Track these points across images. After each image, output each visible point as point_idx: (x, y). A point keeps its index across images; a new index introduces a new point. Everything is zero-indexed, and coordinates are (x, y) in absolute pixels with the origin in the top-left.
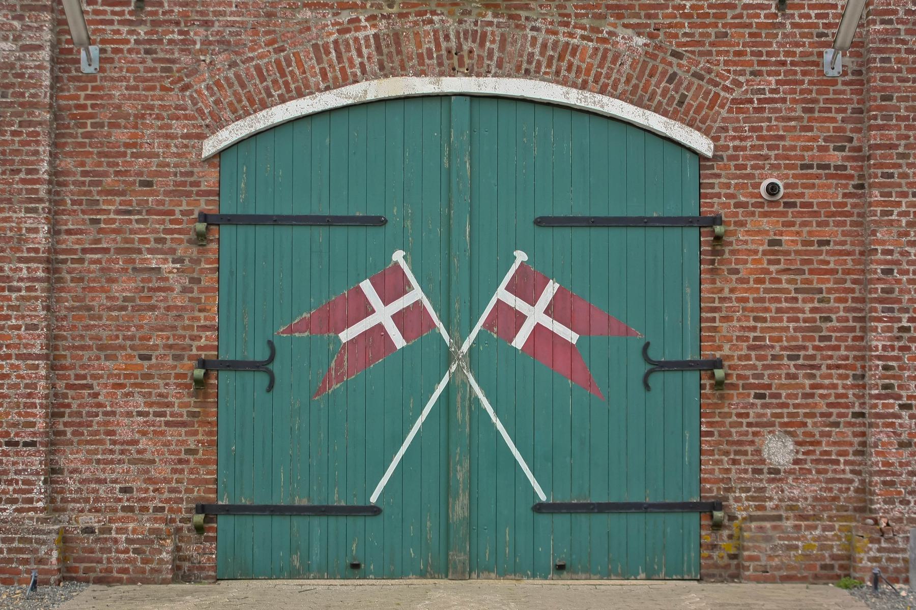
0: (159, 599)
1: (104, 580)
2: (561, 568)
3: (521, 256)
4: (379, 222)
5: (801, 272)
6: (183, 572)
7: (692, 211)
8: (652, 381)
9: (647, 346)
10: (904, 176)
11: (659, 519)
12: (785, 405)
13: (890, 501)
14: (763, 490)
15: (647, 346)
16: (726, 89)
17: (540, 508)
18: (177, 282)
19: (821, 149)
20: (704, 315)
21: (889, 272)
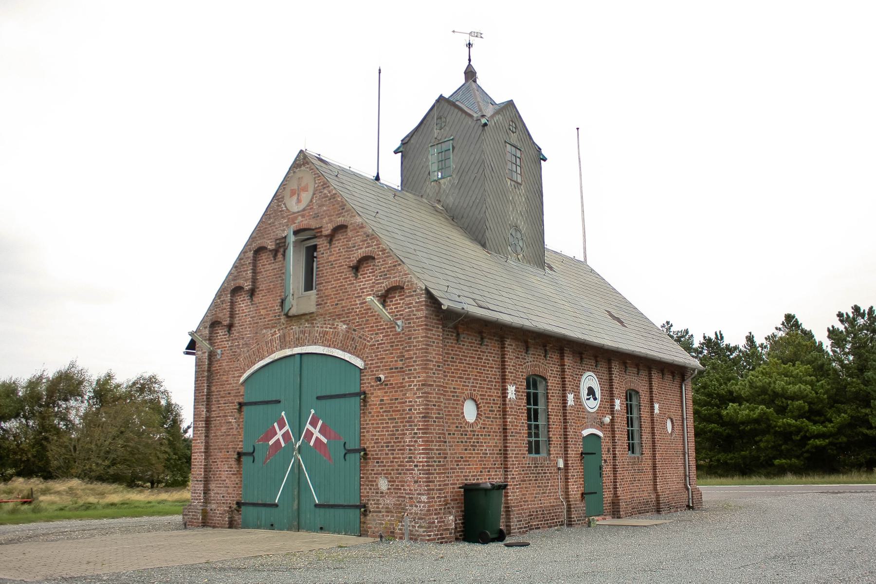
0: (106, 531)
1: (214, 527)
3: (313, 411)
5: (389, 411)
6: (232, 525)
7: (358, 390)
10: (415, 370)
11: (348, 511)
12: (385, 466)
13: (411, 506)
17: (316, 506)
18: (235, 425)
19: (396, 361)
21: (410, 410)
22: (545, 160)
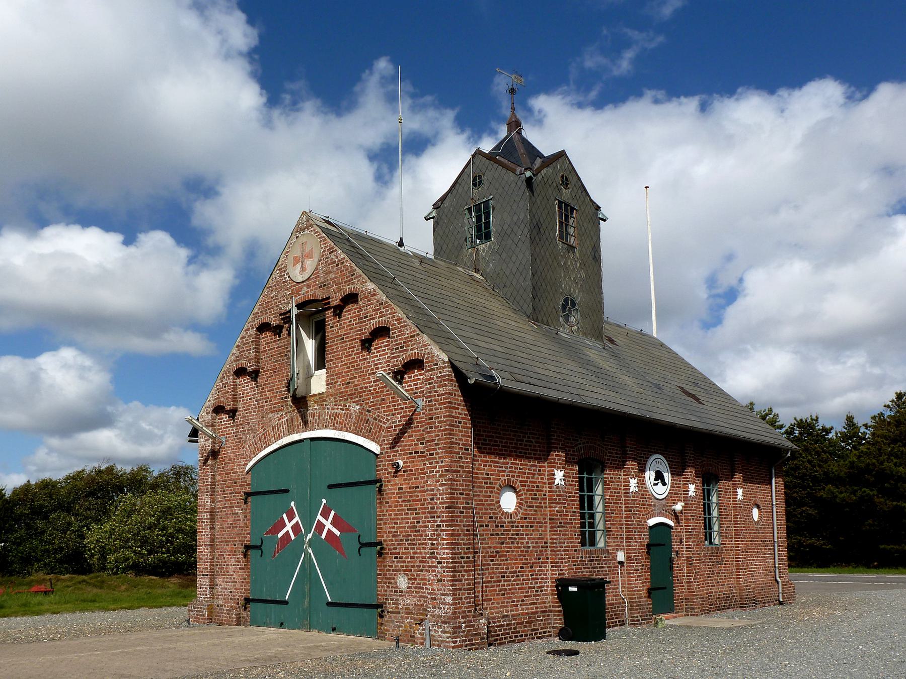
2: (334, 629)
3: (324, 501)
4: (286, 491)
12: (404, 562)
13: (434, 607)
14: (397, 600)
16: (384, 423)
17: (329, 604)
18: (242, 517)
21: (432, 499)
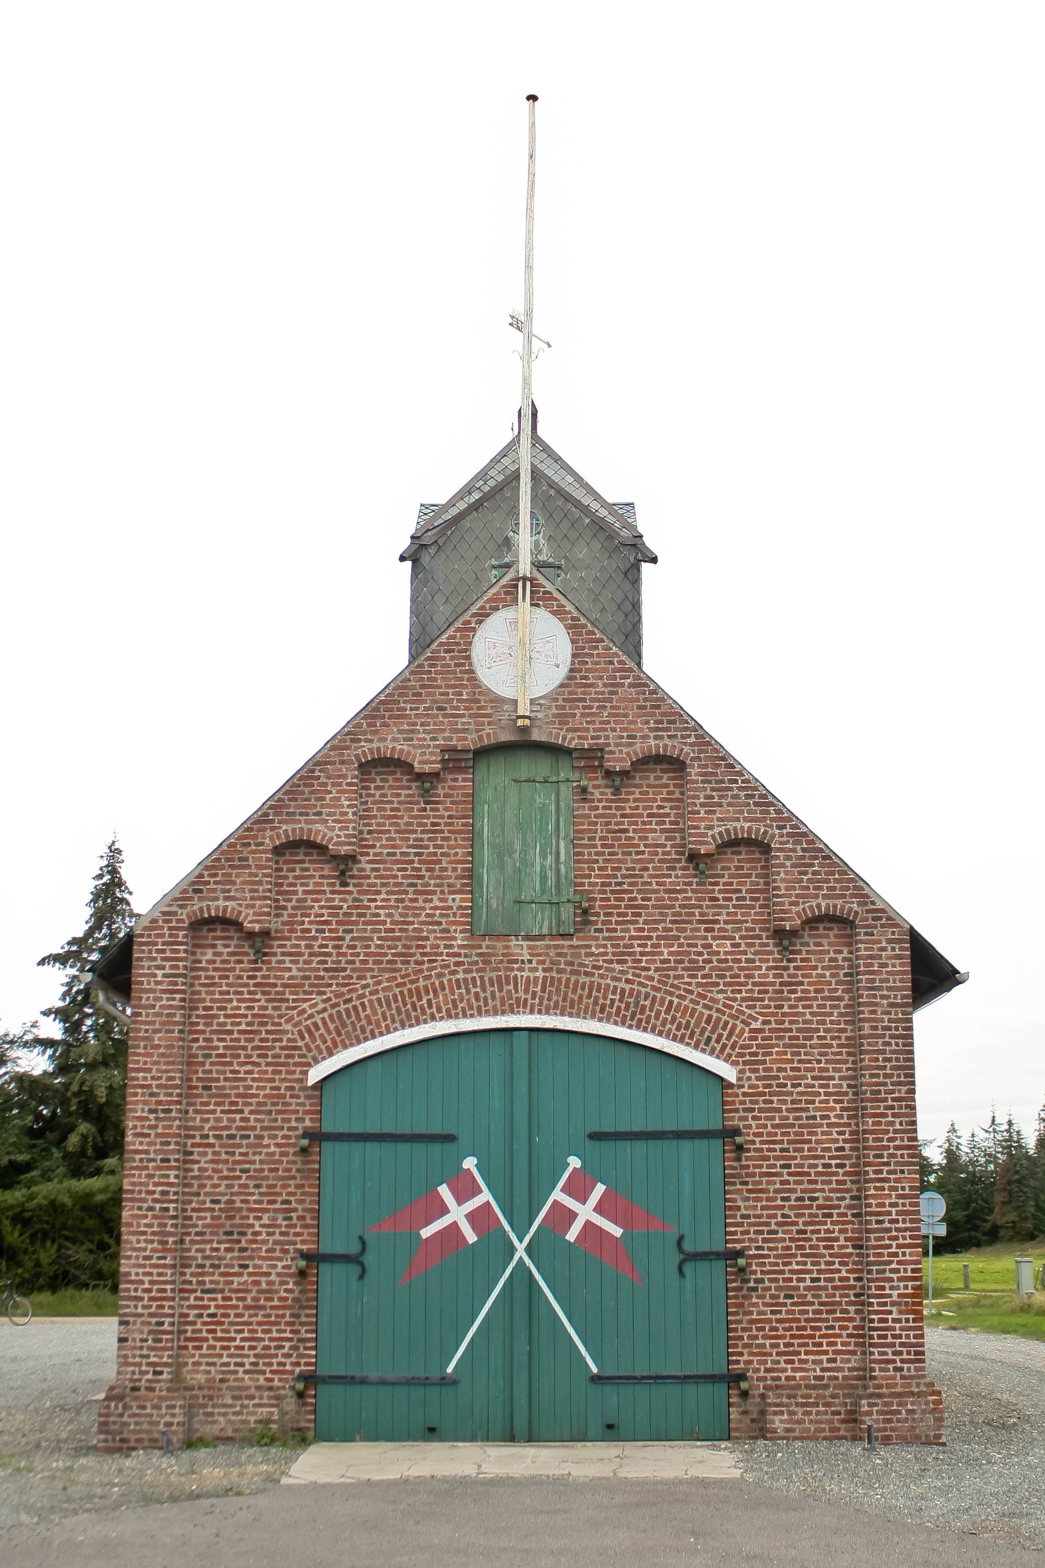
4: (450, 1138)
8: (688, 1268)
9: (362, 1276)
15: (362, 1276)
20: (317, 1166)
22: (654, 560)
